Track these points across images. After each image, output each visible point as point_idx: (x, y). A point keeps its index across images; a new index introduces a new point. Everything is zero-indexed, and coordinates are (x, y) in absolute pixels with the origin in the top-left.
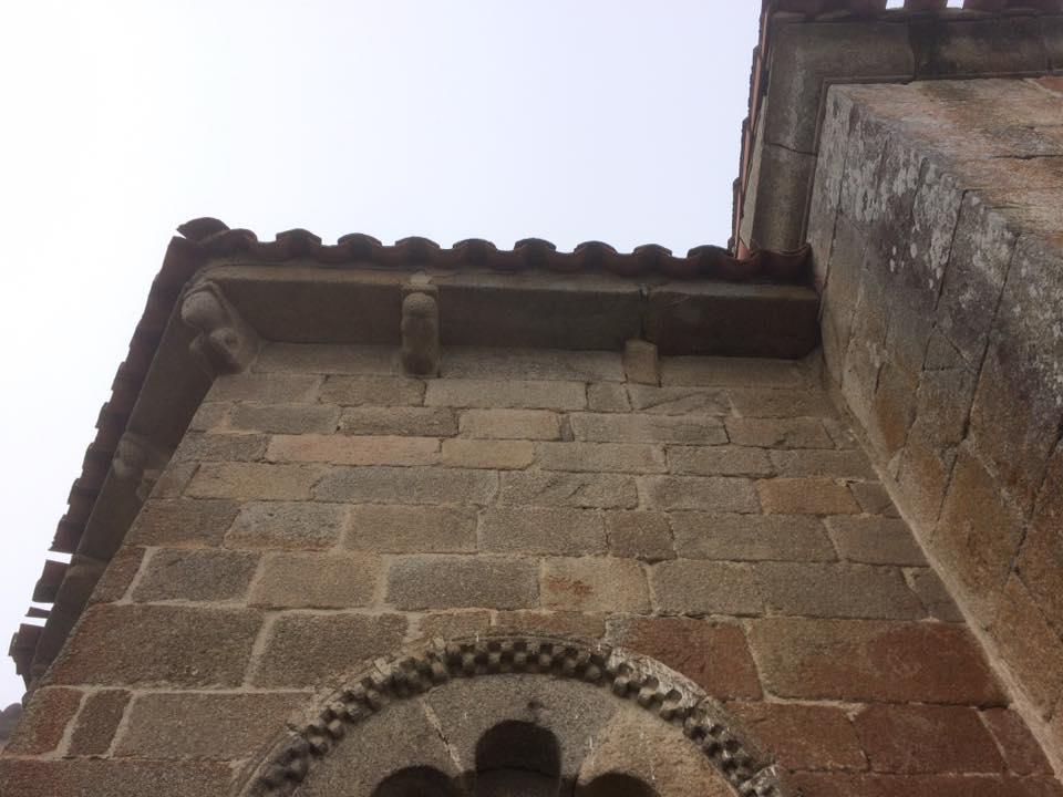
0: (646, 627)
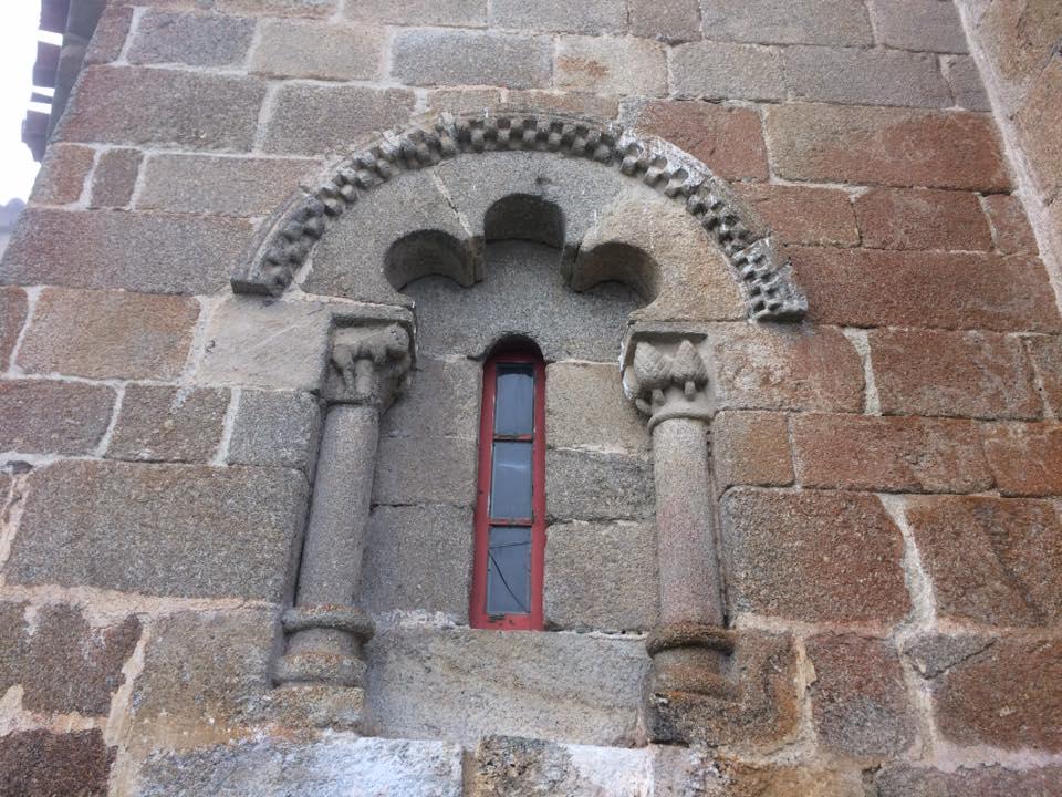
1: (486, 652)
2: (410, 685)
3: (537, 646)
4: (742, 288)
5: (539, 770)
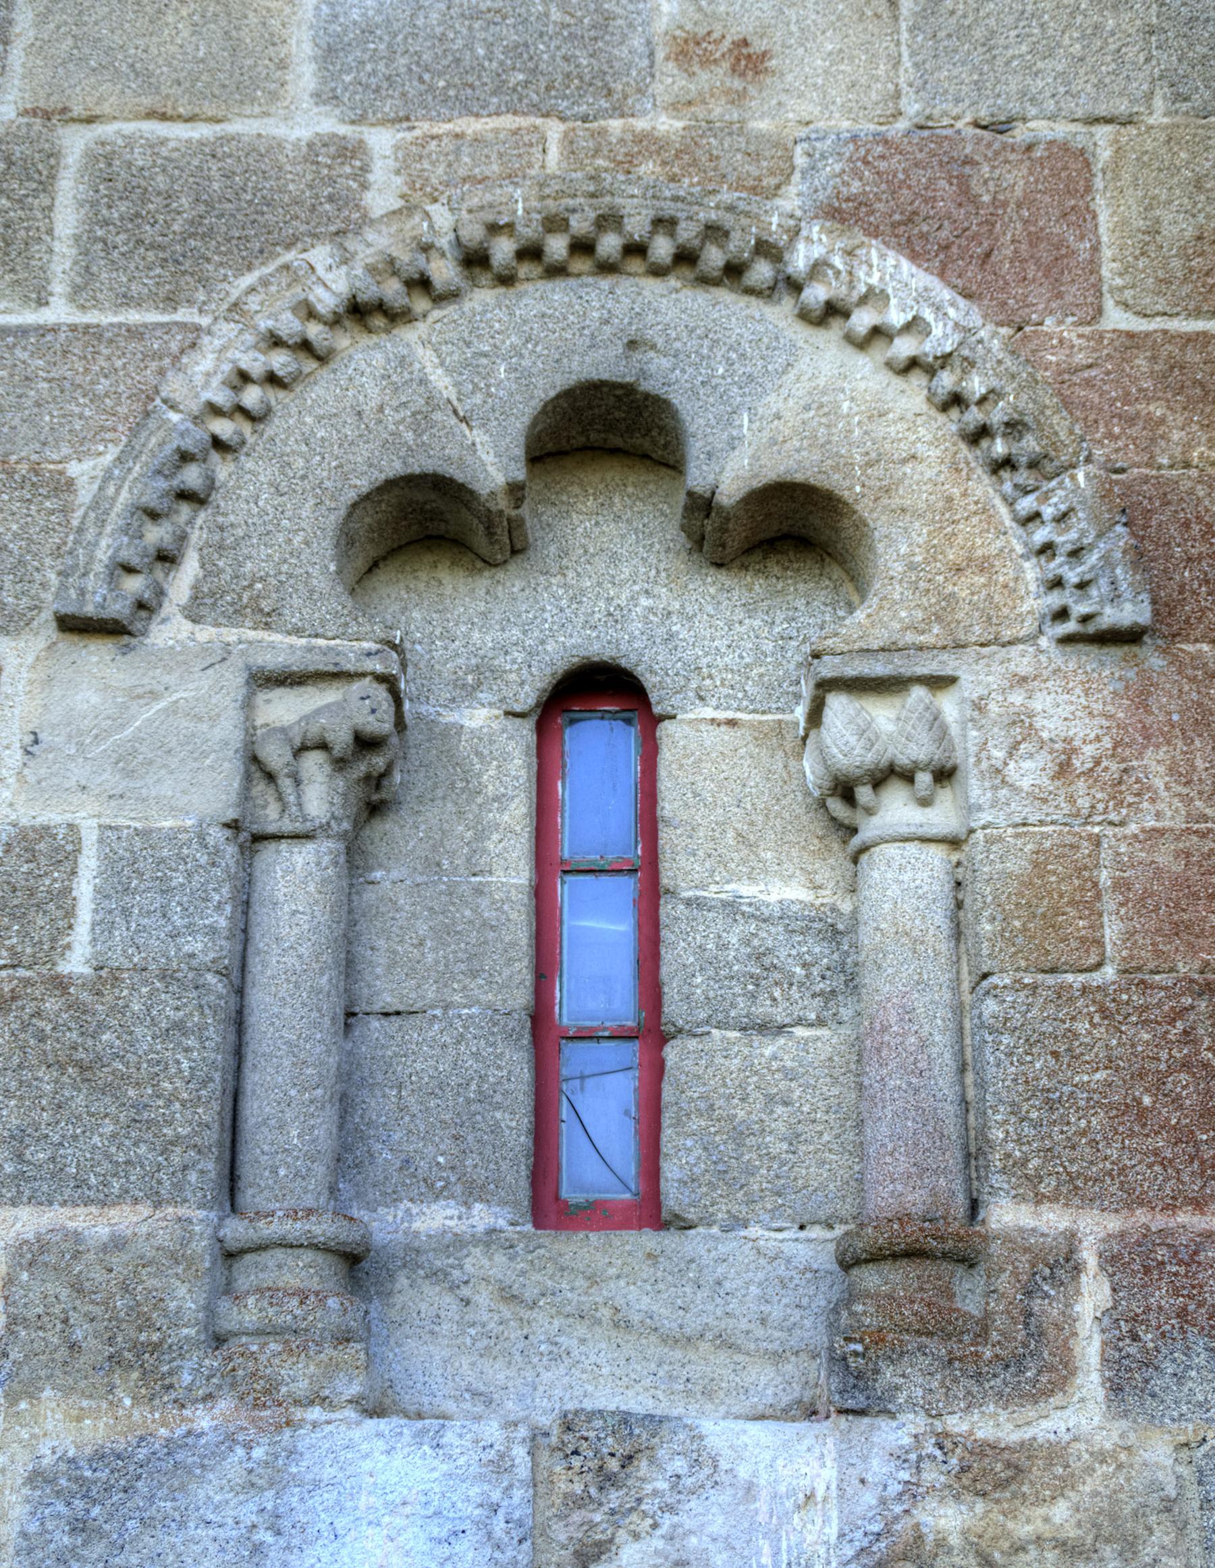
0: (883, 157)
1: (562, 1269)
2: (437, 1329)
3: (650, 1256)
4: (1031, 572)
5: (652, 1460)
